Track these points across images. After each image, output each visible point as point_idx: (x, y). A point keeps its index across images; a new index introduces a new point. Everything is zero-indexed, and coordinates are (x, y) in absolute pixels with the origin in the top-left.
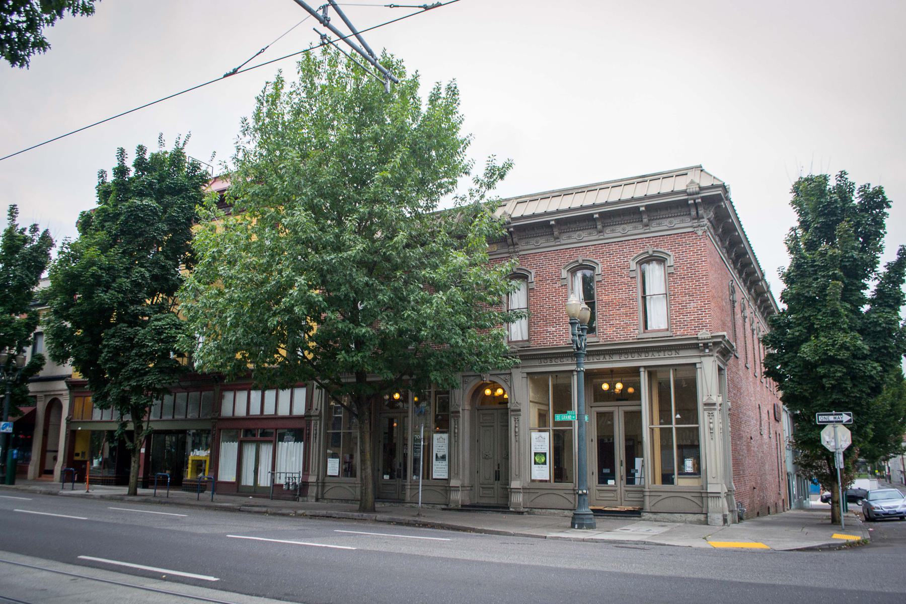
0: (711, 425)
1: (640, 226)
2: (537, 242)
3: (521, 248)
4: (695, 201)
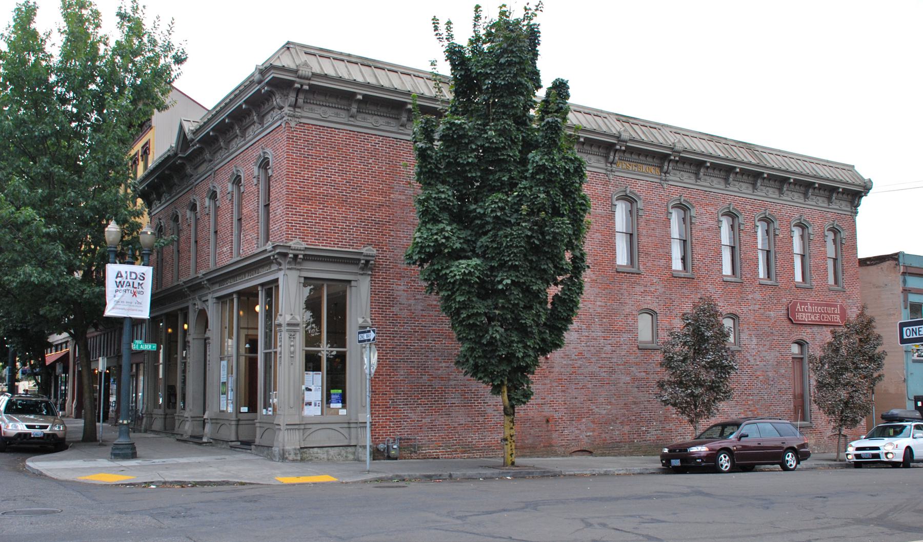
0: (292, 348)
1: (343, 114)
2: (325, 113)
3: (671, 178)
4: (302, 86)
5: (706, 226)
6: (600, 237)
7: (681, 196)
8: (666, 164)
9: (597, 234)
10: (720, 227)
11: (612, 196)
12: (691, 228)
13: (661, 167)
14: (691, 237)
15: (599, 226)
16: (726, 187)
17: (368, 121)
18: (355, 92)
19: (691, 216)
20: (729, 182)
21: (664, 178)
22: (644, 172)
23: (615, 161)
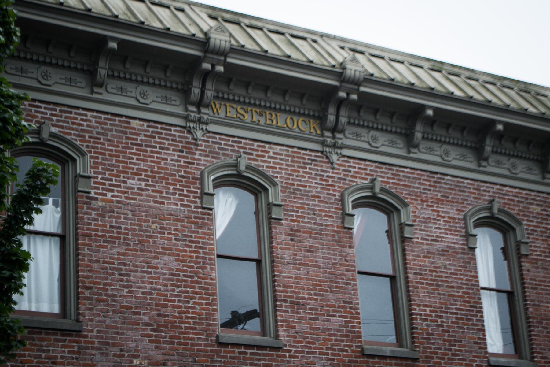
5: (440, 245)
6: (174, 265)
7: (373, 181)
8: (332, 110)
9: (166, 258)
10: (473, 249)
11: (202, 174)
12: (404, 250)
13: (321, 119)
14: (405, 269)
15: (170, 239)
16: (480, 165)
17: (29, 75)
18: (105, 36)
19: (401, 224)
20: (485, 155)
21: (329, 140)
22: (282, 128)
23: (206, 100)
